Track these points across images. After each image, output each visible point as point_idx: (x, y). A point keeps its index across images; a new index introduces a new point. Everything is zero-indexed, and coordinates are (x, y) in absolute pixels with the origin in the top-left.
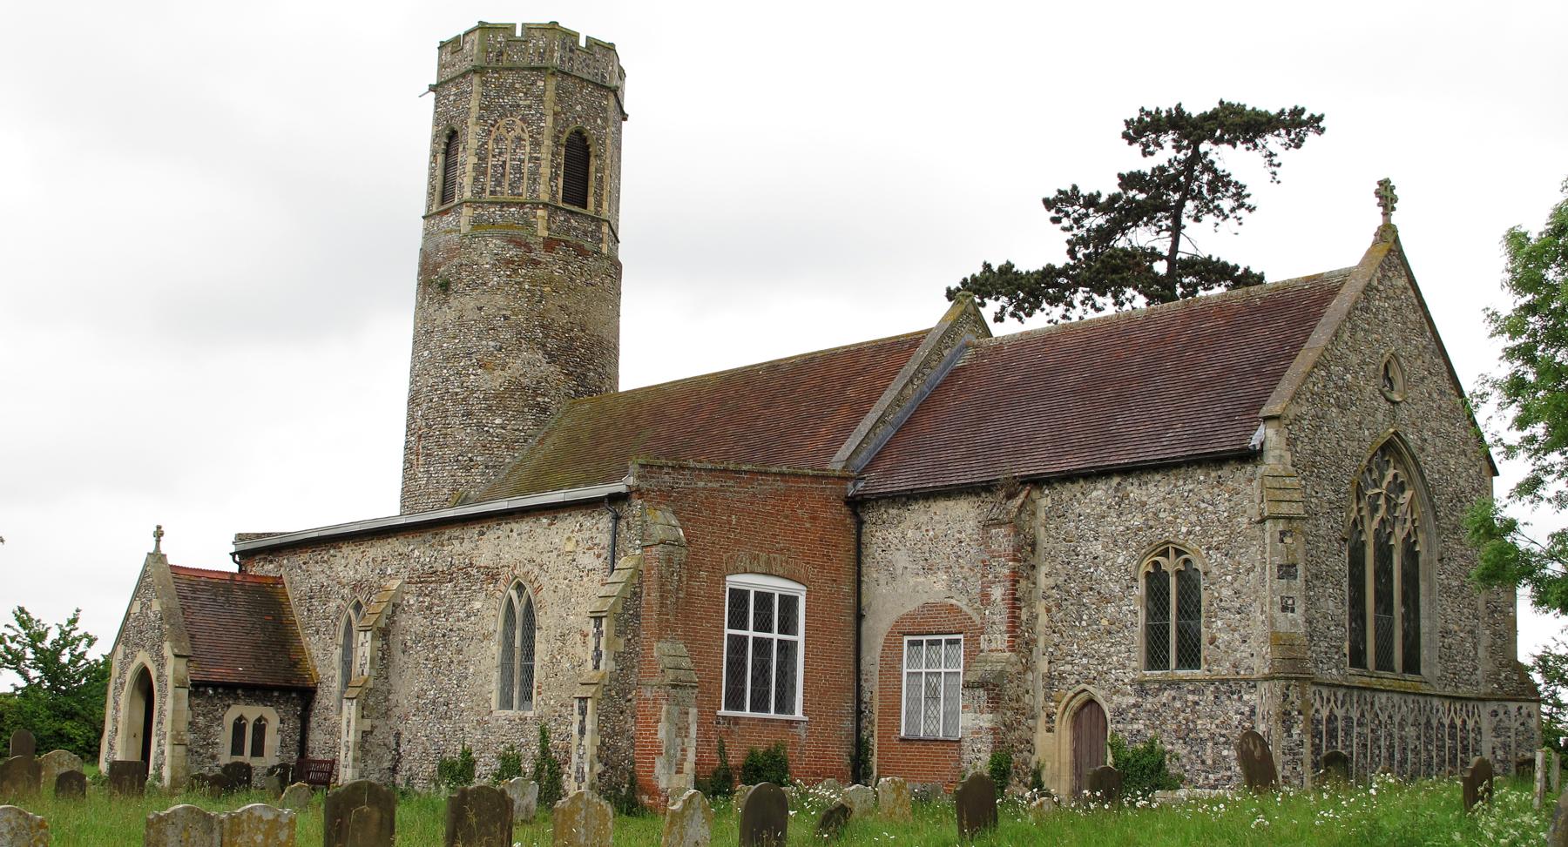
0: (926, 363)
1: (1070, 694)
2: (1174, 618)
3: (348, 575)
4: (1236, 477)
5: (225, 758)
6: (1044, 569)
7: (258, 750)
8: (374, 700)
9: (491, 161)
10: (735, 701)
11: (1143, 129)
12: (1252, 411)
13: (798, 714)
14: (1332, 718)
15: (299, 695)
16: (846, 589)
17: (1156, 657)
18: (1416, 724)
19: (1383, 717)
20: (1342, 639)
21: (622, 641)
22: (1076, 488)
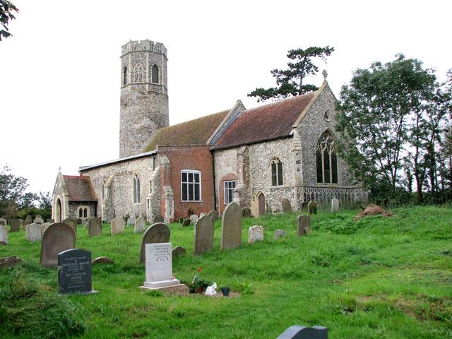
0: (230, 117)
2: (277, 171)
3: (102, 175)
4: (288, 141)
5: (78, 217)
6: (251, 164)
7: (85, 216)
8: (110, 203)
10: (185, 198)
11: (292, 54)
12: (290, 126)
14: (313, 194)
15: (95, 204)
17: (274, 184)
18: (336, 195)
19: (327, 194)
22: (257, 145)
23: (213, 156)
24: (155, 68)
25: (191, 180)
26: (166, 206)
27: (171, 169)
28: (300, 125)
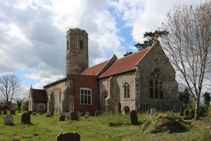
1: (118, 102)
9: (72, 44)
11: (146, 35)
13: (91, 104)
14: (147, 105)
16: (97, 89)
18: (161, 105)
19: (156, 104)
20: (149, 94)
21: (66, 96)
23: (99, 82)
24: (81, 43)
25: (86, 93)
26: (70, 106)
27: (74, 88)
28: (140, 64)
